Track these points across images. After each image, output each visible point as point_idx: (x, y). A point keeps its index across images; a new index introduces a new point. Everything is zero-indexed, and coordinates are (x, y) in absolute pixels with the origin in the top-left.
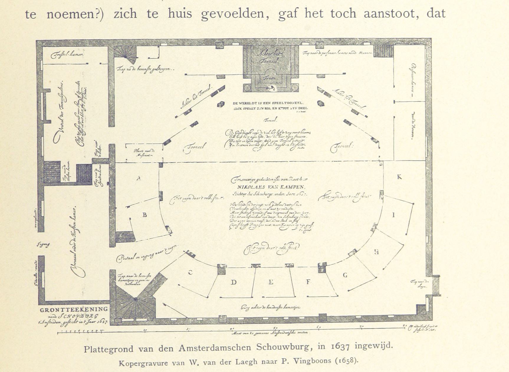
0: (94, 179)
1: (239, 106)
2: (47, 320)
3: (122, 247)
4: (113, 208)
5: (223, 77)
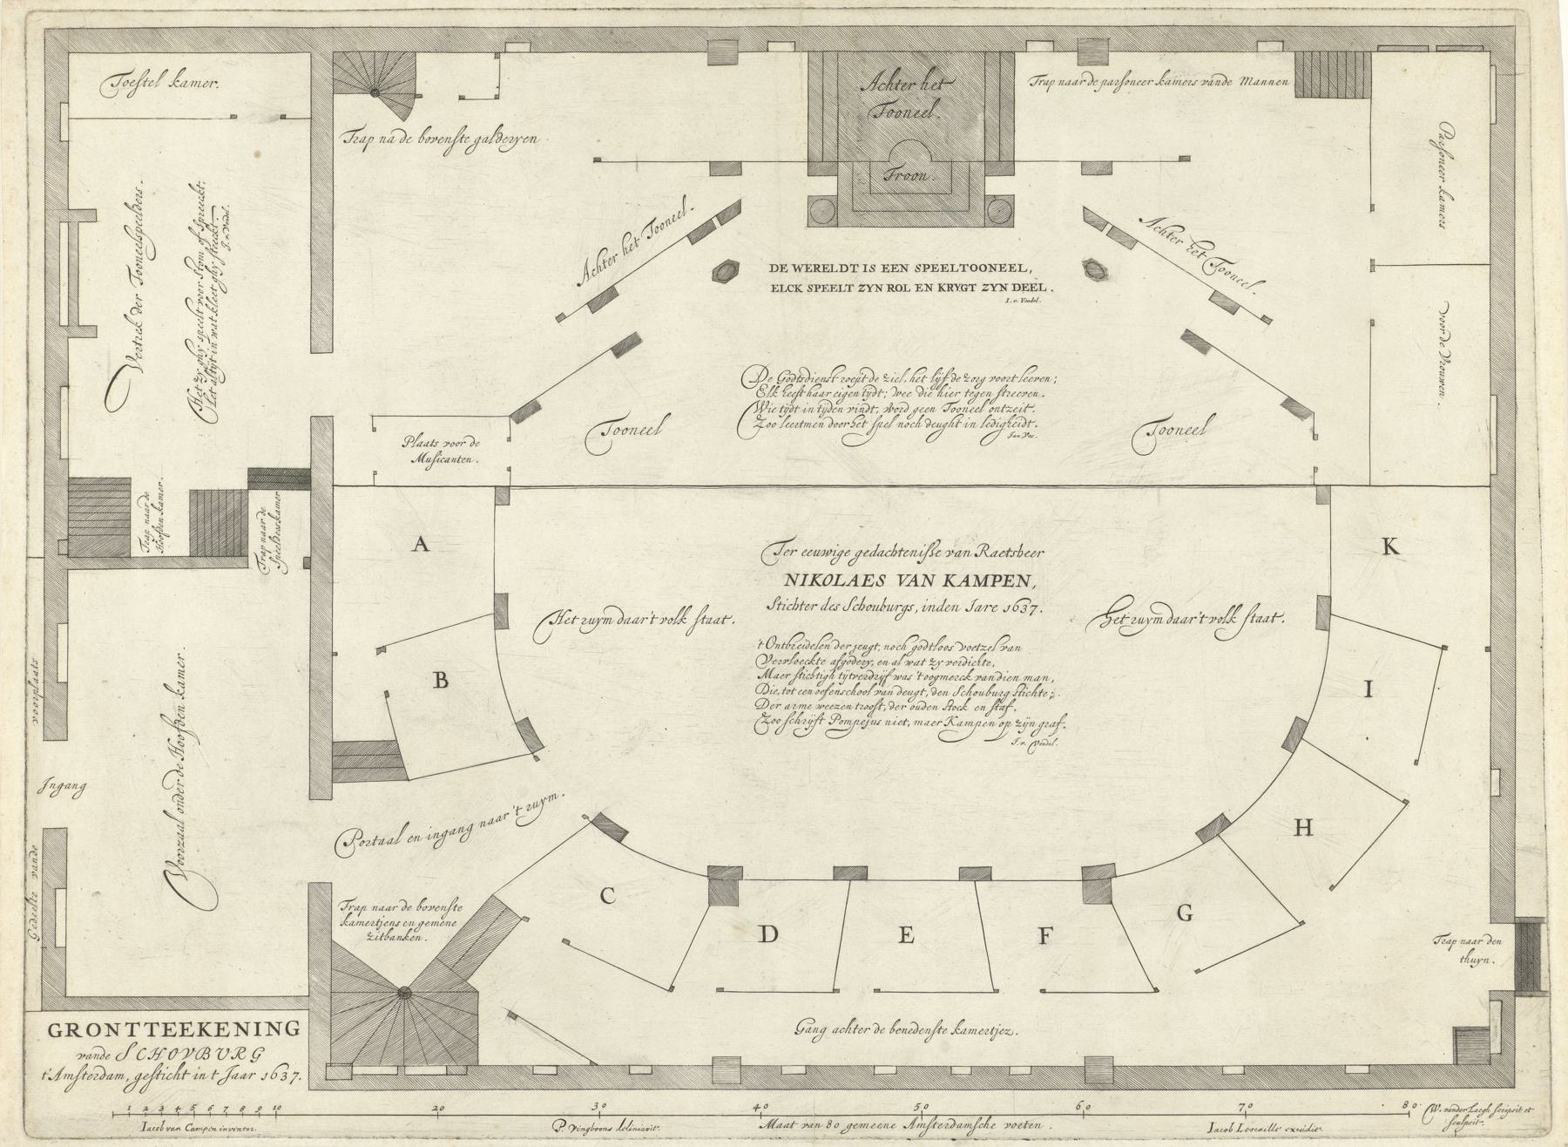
0: (254, 545)
1: (789, 278)
2: (74, 1068)
3: (361, 800)
5: (735, 168)
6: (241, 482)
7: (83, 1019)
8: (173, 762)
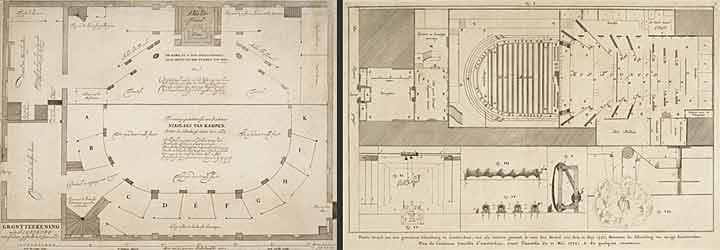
0: (49, 118)
1: (170, 58)
2: (8, 235)
3: (72, 175)
4: (64, 142)
5: (158, 33)
6: (46, 103)
7: (11, 224)
8: (30, 166)
